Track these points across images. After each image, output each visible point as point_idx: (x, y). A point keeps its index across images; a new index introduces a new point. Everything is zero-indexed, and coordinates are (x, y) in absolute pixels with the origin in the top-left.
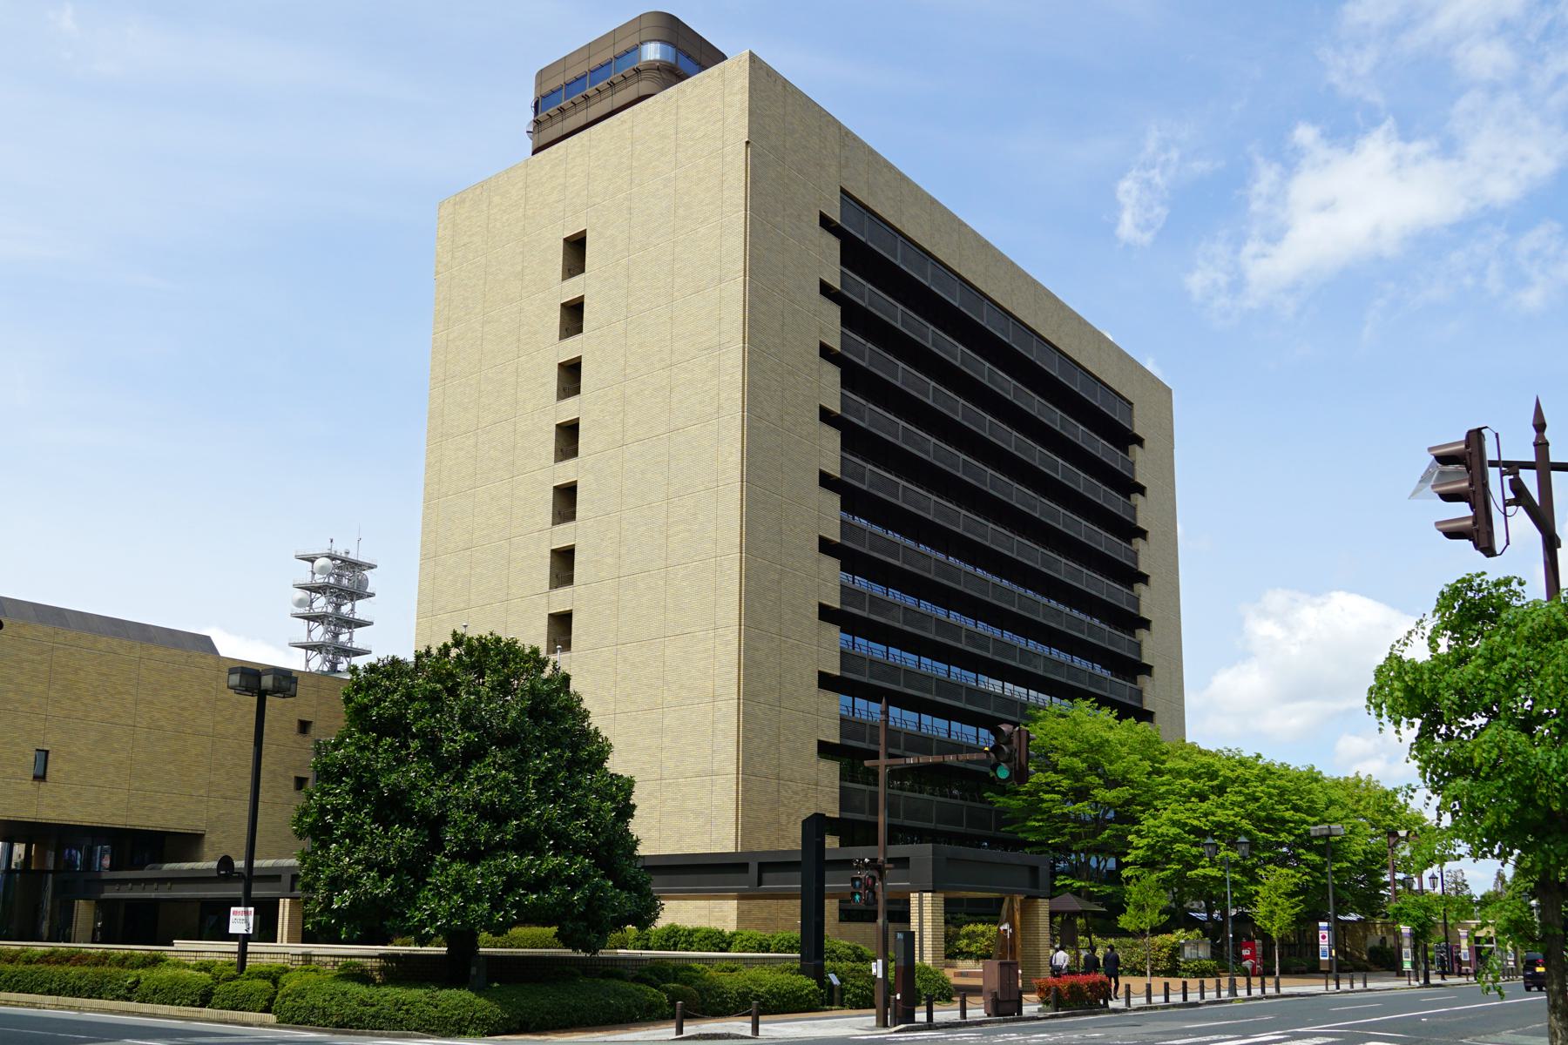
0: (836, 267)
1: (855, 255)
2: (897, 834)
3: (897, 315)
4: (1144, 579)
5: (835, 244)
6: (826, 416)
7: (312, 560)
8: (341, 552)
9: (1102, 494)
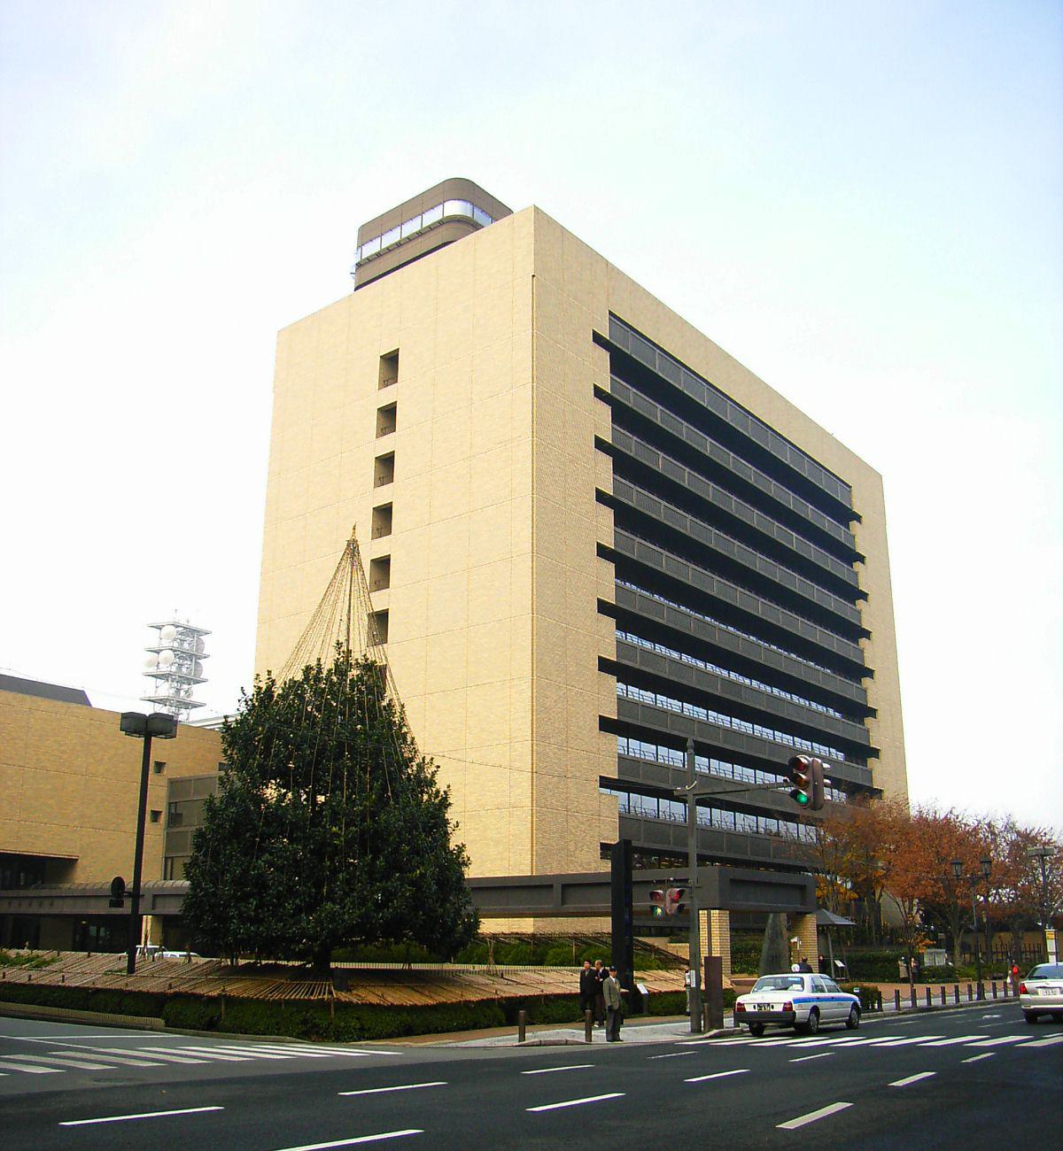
1: (622, 364)
2: (702, 859)
3: (658, 414)
4: (867, 634)
5: (606, 355)
6: (601, 497)
7: (160, 628)
8: (183, 622)
9: (828, 562)
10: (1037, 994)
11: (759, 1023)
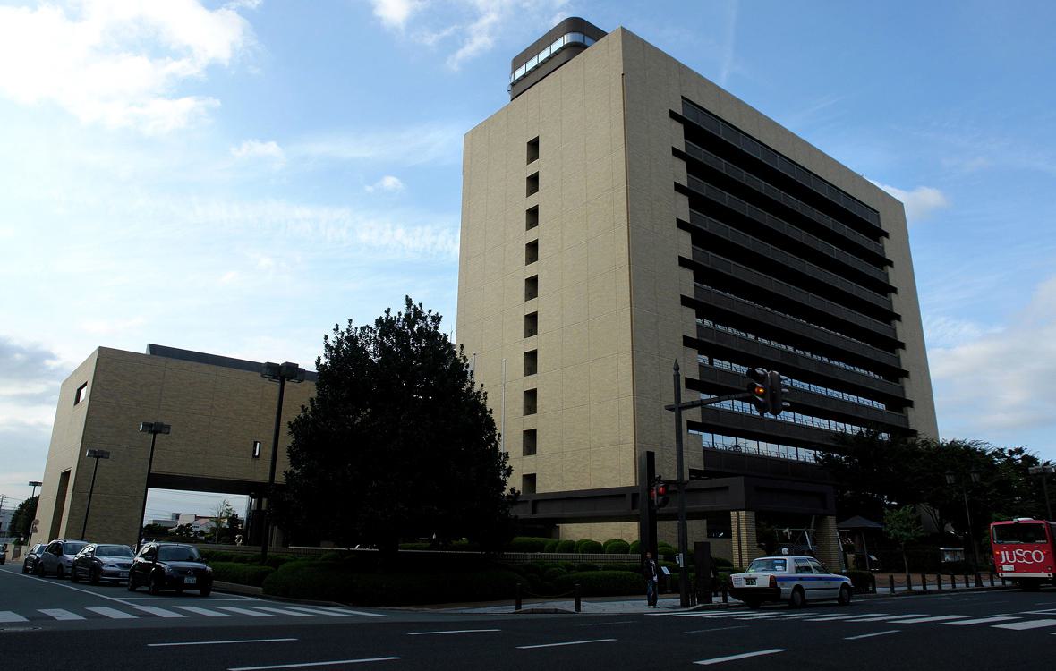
0: (682, 140)
1: (692, 132)
3: (723, 166)
10: (201, 553)
11: (753, 597)
